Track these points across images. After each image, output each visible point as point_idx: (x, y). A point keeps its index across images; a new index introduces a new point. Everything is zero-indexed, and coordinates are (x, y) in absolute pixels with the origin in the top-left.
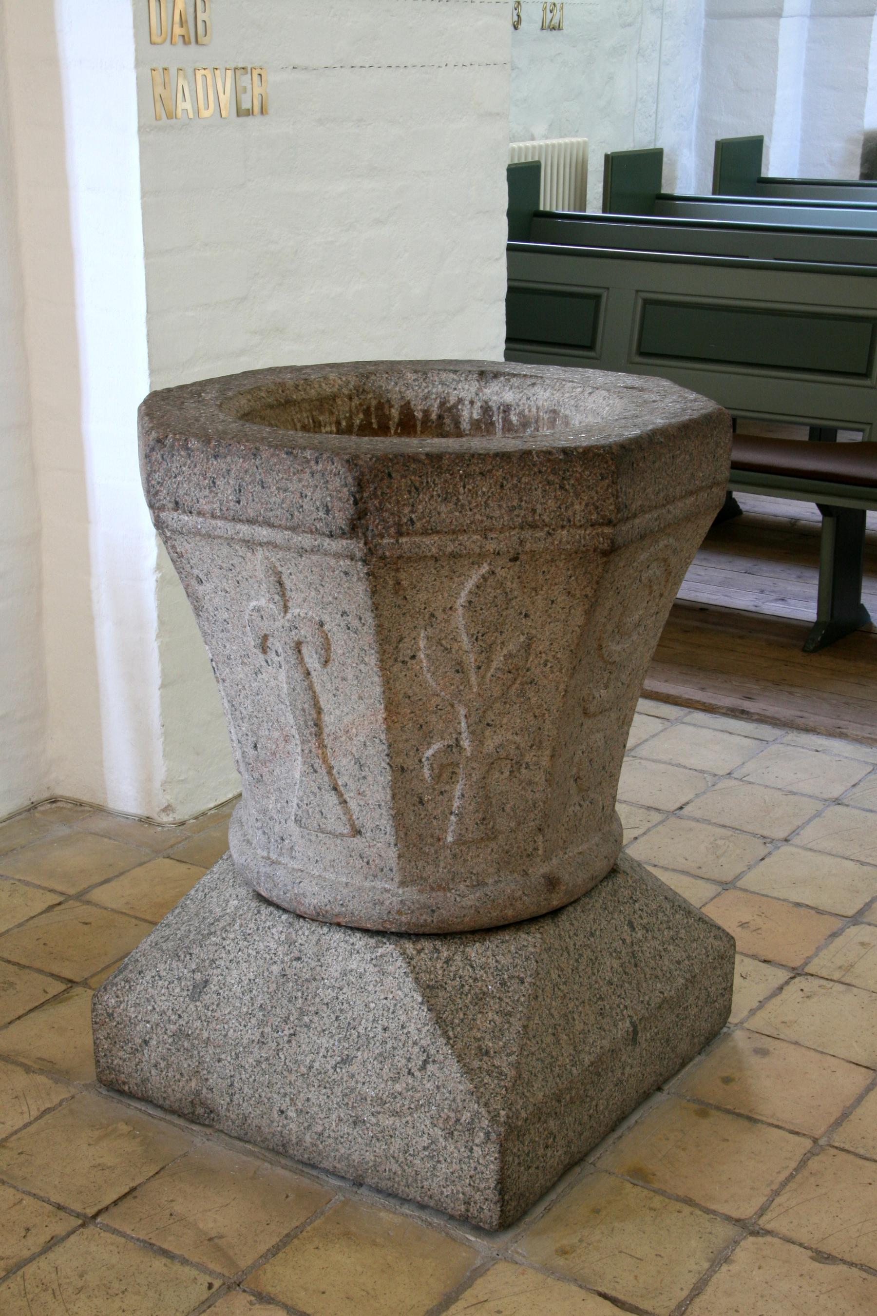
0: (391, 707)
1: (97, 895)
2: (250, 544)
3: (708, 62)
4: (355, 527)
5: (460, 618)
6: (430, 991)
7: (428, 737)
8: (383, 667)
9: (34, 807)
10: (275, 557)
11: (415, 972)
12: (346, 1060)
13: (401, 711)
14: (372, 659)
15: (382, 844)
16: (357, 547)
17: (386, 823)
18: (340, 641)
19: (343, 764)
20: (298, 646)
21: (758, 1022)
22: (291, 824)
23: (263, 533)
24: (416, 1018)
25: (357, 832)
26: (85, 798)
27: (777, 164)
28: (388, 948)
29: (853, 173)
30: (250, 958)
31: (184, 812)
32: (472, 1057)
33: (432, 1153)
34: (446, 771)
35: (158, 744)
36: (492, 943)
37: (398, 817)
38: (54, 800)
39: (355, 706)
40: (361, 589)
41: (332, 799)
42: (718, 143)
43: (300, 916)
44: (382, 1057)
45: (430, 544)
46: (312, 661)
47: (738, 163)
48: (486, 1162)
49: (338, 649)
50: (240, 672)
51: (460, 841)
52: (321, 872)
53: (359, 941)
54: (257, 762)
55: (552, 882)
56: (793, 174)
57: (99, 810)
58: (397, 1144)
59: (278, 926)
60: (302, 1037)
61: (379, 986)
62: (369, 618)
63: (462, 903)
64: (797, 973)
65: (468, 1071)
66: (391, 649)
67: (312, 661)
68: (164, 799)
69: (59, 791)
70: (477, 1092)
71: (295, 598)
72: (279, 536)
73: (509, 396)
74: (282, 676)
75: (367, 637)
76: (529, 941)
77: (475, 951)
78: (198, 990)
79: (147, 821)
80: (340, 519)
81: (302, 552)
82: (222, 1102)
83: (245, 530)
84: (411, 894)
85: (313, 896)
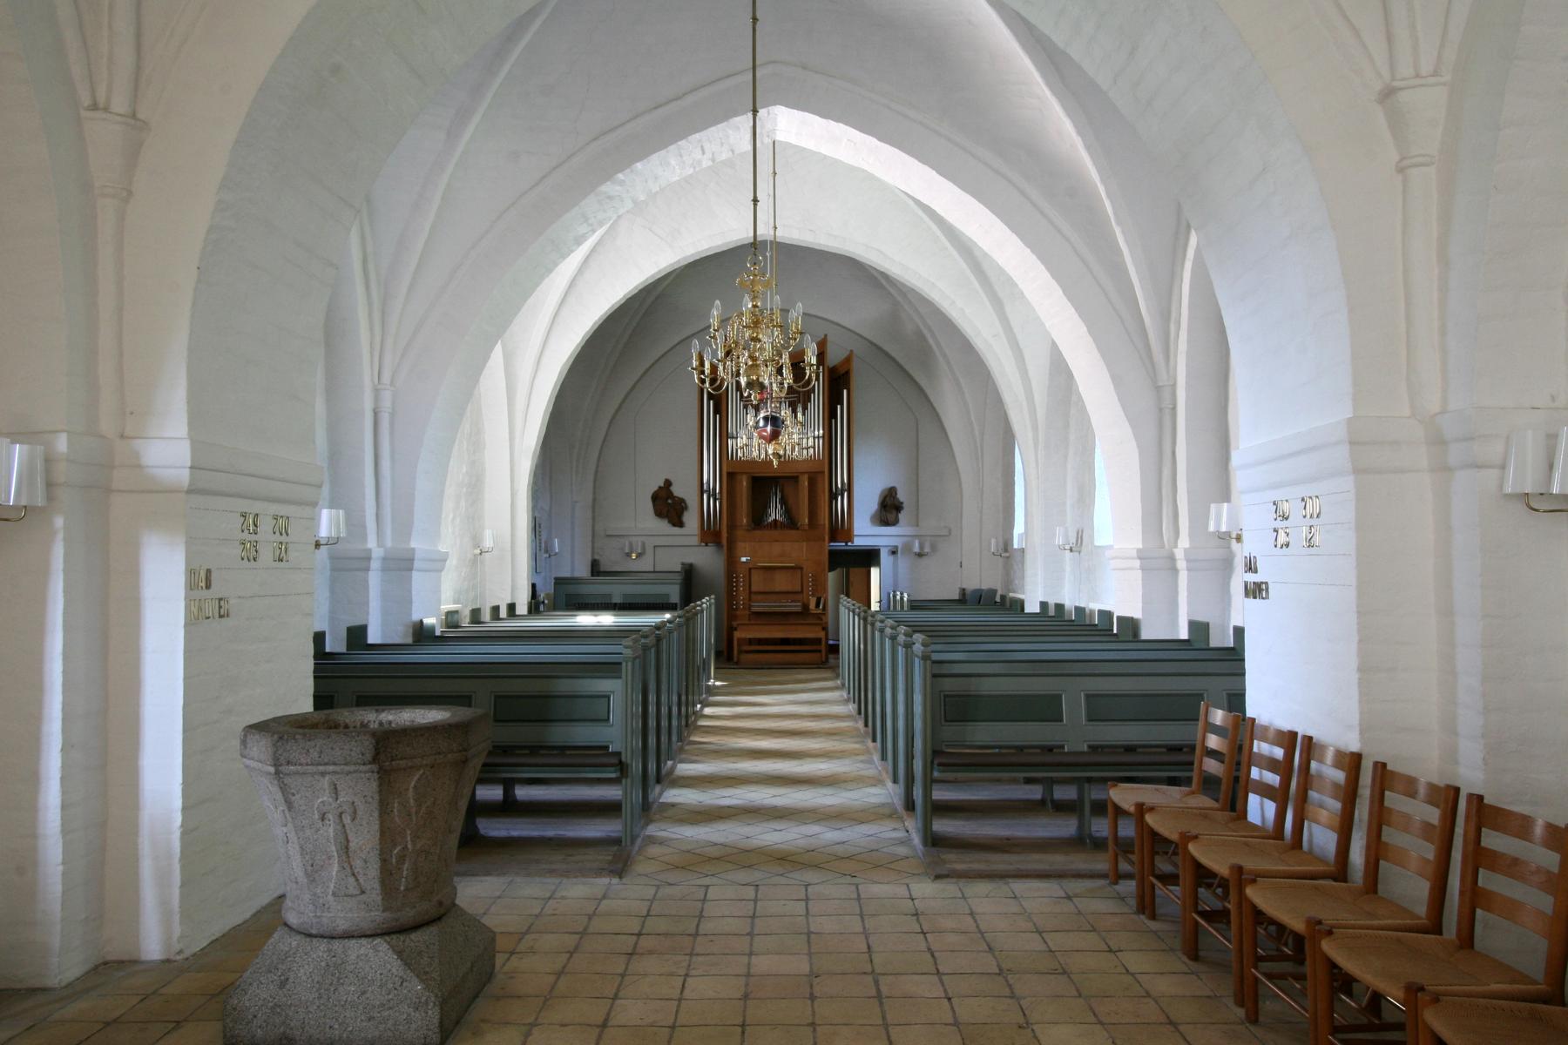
0: (382, 833)
1: (163, 991)
2: (323, 774)
3: (332, 591)
4: (375, 760)
5: (411, 793)
6: (400, 954)
7: (395, 846)
8: (381, 816)
9: (96, 968)
10: (334, 778)
11: (392, 947)
12: (364, 993)
13: (388, 836)
14: (376, 814)
15: (375, 895)
16: (375, 767)
17: (377, 886)
18: (361, 807)
19: (358, 863)
20: (340, 815)
21: (506, 969)
22: (330, 897)
23: (331, 768)
24: (395, 966)
25: (363, 892)
26: (126, 958)
27: (373, 637)
28: (378, 940)
29: (410, 640)
30: (309, 962)
31: (187, 953)
32: (423, 976)
33: (408, 1021)
34: (402, 858)
35: (177, 918)
36: (419, 933)
37: (383, 882)
38: (105, 963)
39: (365, 838)
40: (375, 785)
41: (352, 880)
42: (349, 629)
43: (333, 938)
44: (381, 986)
45: (403, 763)
46: (347, 819)
47: (357, 635)
48: (434, 1014)
49: (359, 813)
50: (308, 832)
51: (407, 889)
52: (343, 915)
53: (364, 941)
54: (313, 872)
55: (440, 903)
56: (379, 641)
57: (135, 962)
58: (391, 1022)
59: (323, 945)
60: (341, 989)
61: (378, 958)
62: (377, 797)
63: (408, 915)
64: (512, 953)
65: (422, 981)
66: (384, 808)
67: (347, 819)
68: (178, 947)
69: (109, 958)
70: (427, 988)
71: (342, 793)
72: (337, 768)
73: (391, 718)
74: (331, 830)
75: (375, 804)
76: (433, 929)
77: (413, 936)
78: (283, 985)
79: (168, 961)
80: (369, 757)
81: (349, 773)
82: (297, 1033)
83: (321, 768)
84: (387, 915)
85: (342, 925)
